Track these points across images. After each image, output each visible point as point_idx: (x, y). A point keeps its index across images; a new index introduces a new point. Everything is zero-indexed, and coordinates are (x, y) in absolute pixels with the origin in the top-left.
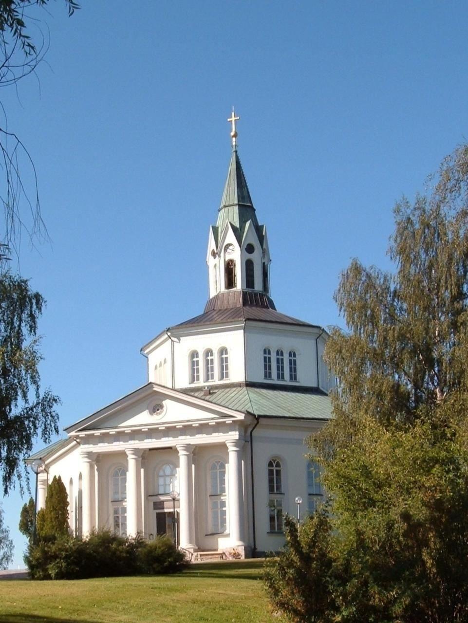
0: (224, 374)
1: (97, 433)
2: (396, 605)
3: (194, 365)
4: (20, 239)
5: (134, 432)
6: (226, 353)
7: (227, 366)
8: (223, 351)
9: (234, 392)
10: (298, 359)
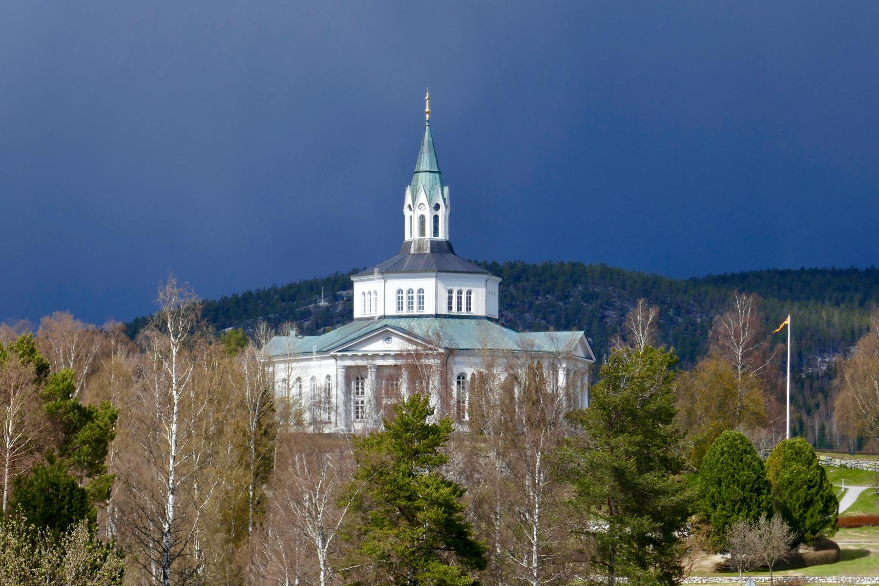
0: (421, 307)
1: (349, 354)
2: (78, 323)
3: (400, 299)
4: (430, 172)
5: (385, 355)
6: (423, 293)
7: (423, 302)
8: (421, 291)
9: (424, 323)
10: (425, 294)
